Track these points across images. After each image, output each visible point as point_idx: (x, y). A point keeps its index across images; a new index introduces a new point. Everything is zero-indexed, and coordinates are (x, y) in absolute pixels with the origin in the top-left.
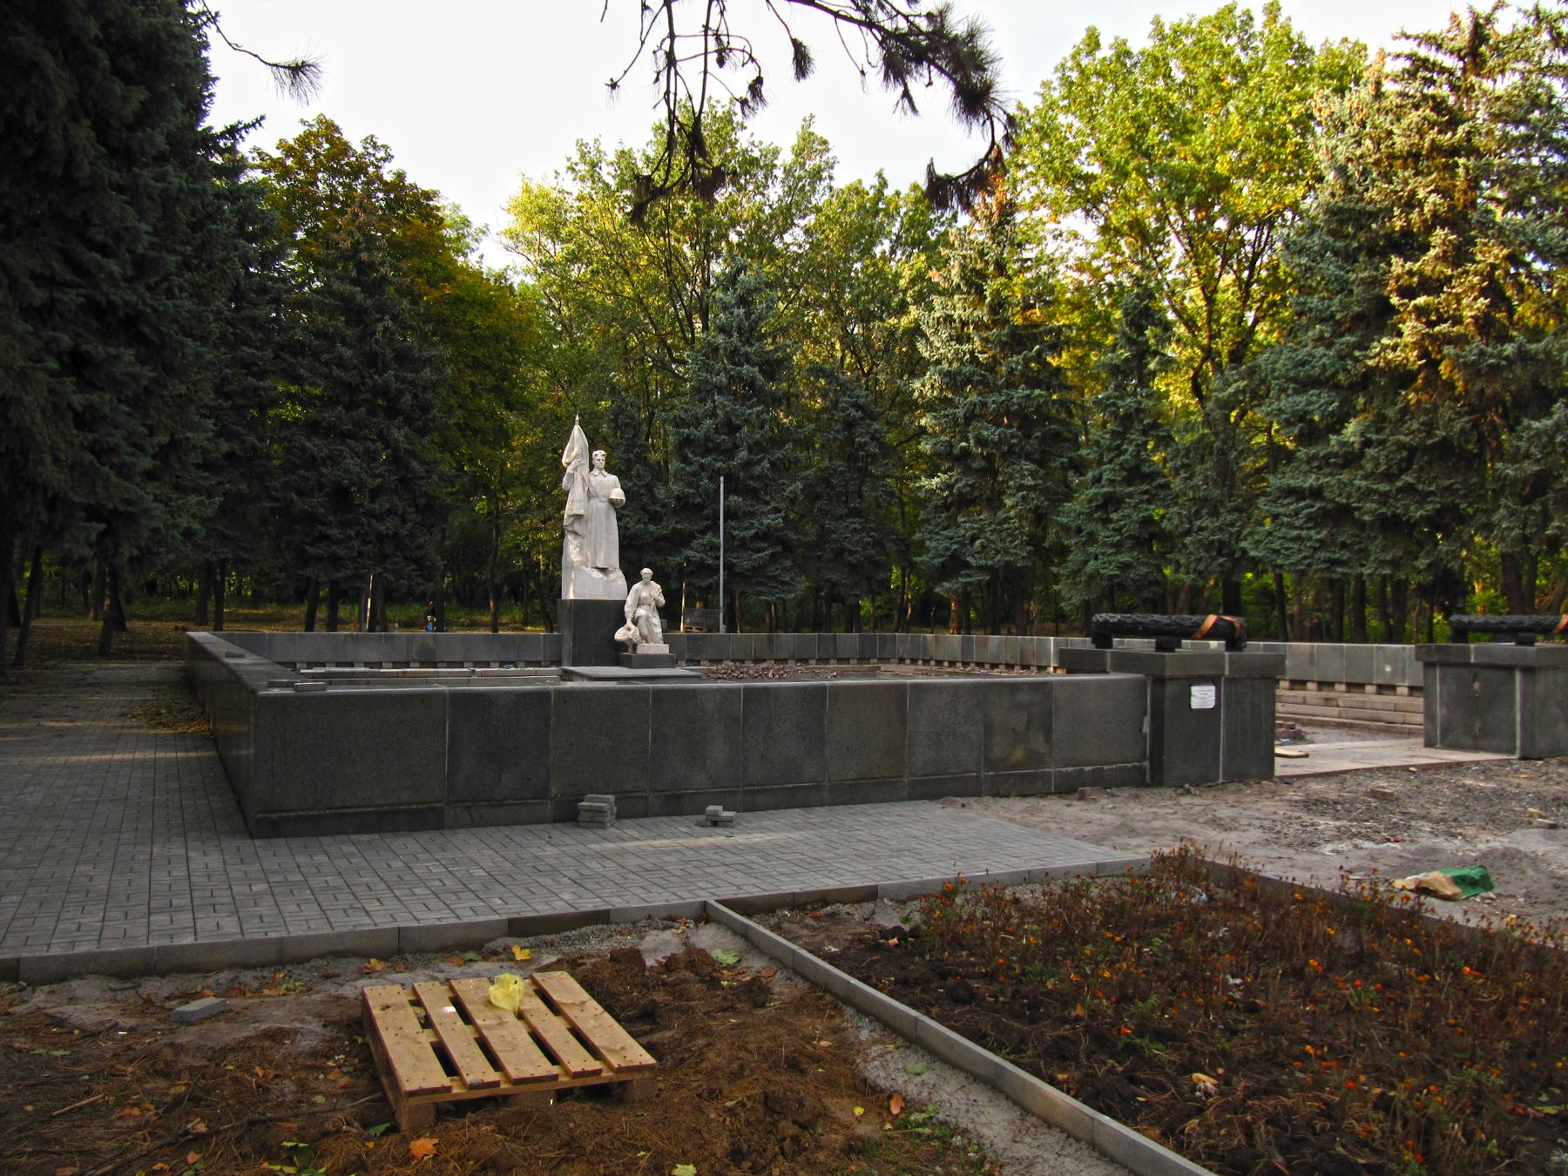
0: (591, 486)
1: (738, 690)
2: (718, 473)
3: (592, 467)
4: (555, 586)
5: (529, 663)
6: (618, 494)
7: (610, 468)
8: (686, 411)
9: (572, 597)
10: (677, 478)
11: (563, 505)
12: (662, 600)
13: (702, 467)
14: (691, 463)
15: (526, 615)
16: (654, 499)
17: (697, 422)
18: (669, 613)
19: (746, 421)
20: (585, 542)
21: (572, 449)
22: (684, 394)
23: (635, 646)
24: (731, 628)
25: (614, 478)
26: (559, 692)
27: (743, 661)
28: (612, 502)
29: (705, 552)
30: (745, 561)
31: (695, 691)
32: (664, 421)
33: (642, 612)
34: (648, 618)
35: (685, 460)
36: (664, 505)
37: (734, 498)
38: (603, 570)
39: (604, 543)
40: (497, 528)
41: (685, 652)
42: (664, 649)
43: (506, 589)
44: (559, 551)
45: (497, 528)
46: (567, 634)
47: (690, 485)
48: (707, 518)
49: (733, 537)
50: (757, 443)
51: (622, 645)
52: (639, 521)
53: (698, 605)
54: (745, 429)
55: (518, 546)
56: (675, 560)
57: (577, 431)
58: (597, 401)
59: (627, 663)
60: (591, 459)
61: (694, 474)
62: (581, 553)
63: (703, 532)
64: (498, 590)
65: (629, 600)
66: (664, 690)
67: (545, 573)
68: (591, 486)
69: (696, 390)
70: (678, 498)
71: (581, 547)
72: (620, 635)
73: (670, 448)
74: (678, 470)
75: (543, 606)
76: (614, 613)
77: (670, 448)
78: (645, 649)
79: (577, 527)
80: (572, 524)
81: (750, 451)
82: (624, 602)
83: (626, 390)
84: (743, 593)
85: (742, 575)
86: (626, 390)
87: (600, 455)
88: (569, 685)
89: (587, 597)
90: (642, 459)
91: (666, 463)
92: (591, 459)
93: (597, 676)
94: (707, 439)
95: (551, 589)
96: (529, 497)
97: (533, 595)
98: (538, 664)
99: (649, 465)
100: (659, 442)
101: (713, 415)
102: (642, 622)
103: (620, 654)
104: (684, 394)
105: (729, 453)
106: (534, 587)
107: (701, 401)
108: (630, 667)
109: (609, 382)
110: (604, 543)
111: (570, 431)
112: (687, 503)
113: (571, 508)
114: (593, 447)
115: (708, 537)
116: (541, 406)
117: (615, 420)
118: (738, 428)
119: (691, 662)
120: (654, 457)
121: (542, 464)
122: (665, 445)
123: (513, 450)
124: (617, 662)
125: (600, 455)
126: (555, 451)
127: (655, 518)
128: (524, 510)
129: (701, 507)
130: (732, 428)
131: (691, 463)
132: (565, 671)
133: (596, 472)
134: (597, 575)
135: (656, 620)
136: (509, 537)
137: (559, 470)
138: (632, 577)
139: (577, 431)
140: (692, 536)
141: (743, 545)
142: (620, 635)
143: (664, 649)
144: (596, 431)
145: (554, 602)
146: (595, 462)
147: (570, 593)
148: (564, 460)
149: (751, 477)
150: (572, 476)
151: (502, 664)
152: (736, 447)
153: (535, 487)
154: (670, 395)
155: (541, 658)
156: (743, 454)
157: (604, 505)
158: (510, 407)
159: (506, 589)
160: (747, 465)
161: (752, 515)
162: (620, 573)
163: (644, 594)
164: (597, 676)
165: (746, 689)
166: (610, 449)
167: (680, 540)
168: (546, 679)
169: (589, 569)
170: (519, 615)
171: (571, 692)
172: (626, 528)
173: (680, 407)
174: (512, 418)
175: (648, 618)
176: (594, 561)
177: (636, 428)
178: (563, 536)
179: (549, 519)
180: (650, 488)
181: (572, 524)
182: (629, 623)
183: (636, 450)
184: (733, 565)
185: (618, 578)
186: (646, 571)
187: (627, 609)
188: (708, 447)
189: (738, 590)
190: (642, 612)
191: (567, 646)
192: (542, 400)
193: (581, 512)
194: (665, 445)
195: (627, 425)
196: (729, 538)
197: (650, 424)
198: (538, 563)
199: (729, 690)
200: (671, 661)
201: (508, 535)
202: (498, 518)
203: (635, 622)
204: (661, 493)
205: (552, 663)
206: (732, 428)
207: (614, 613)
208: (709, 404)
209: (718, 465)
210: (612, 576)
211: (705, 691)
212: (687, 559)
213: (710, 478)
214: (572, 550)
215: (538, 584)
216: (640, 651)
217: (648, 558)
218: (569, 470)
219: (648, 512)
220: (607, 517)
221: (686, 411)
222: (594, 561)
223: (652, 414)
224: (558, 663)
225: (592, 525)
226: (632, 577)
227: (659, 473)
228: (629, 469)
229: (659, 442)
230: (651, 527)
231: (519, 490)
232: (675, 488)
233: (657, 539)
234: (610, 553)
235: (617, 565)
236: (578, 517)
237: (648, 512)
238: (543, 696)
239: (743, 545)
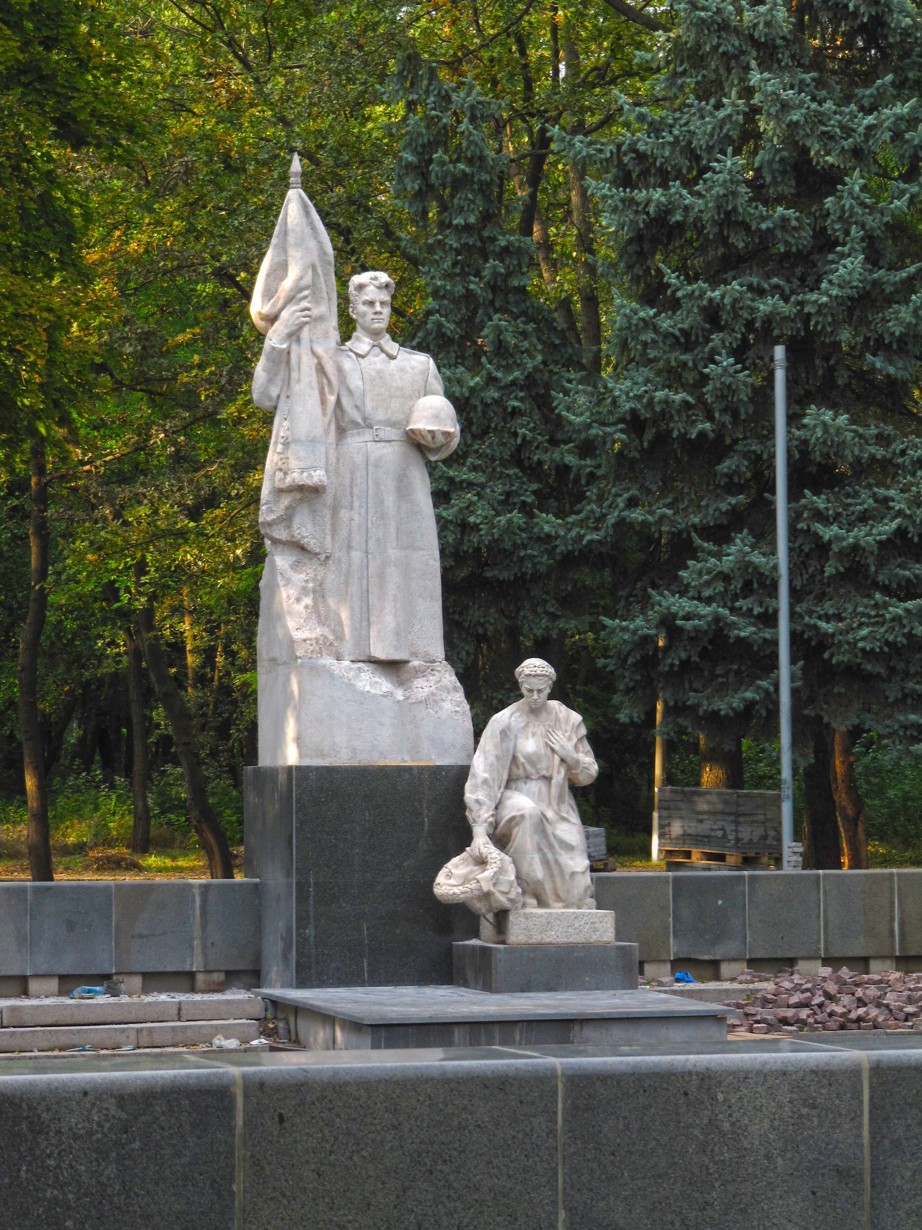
0: (347, 394)
1: (854, 1072)
2: (766, 332)
3: (347, 327)
4: (232, 721)
5: (154, 980)
6: (435, 413)
7: (407, 330)
8: (655, 129)
9: (292, 756)
10: (631, 354)
11: (253, 456)
12: (589, 764)
13: (713, 315)
14: (674, 304)
15: (143, 817)
16: (555, 429)
17: (694, 165)
18: (613, 806)
19: (857, 153)
20: (332, 578)
21: (281, 269)
22: (648, 70)
23: (501, 917)
24: (822, 853)
25: (422, 362)
26: (258, 1088)
27: (862, 963)
28: (418, 444)
29: (728, 599)
30: (861, 626)
31: (707, 1079)
32: (582, 168)
33: (522, 802)
34: (541, 825)
35: (654, 293)
36: (587, 448)
37: (821, 418)
38: (392, 667)
39: (394, 575)
40: (42, 529)
41: (680, 935)
42: (597, 926)
43: (74, 734)
44: (247, 606)
45: (42, 529)
46: (276, 879)
47: (673, 377)
48: (732, 486)
49: (822, 548)
50: (897, 228)
51: (459, 916)
52: (507, 502)
53: (710, 776)
54: (856, 181)
55: (111, 592)
56: (630, 627)
57: (295, 207)
58: (357, 108)
59: (479, 972)
60: (344, 302)
61: (686, 341)
62: (319, 613)
63: (720, 534)
64: (49, 735)
65: (480, 765)
66: (905, 874)
67: (202, 680)
68: (347, 394)
69: (689, 56)
70: (634, 423)
71: (319, 592)
72: (452, 880)
73: (606, 252)
74: (631, 329)
75: (199, 789)
76: (433, 809)
77: (606, 252)
78: (531, 926)
79: (304, 528)
80: (287, 519)
81: (873, 258)
82: (462, 773)
83: (454, 65)
84: (856, 733)
85: (852, 672)
86: (454, 65)
87: (372, 285)
88: (290, 1062)
89: (343, 758)
90: (507, 295)
91: (591, 301)
92: (344, 302)
93: (355, 1034)
94: (729, 219)
95: (223, 731)
96: (144, 431)
97: (164, 751)
98: (186, 980)
99: (537, 316)
100: (564, 236)
101: (747, 136)
102: (524, 837)
103: (448, 942)
104: (648, 70)
105: (804, 264)
106: (155, 724)
107: (703, 94)
108: (488, 987)
109: (394, 39)
110: (394, 575)
111: (271, 210)
112: (663, 438)
113: (291, 458)
114: (349, 257)
115: (739, 547)
116: (177, 126)
117: (421, 170)
118: (831, 180)
119: (685, 965)
120: (551, 284)
121: (182, 321)
122: (586, 244)
123: (86, 277)
124: (445, 971)
125: (372, 285)
126: (224, 276)
127: (561, 490)
128: (130, 471)
129: (711, 449)
130: (810, 181)
131: (674, 304)
132: (275, 1004)
133: (361, 343)
134: (372, 683)
135: (570, 829)
136: (81, 563)
137: (237, 341)
138: (488, 689)
139: (295, 207)
140: (683, 549)
141: (856, 573)
142: (452, 880)
143: (597, 926)
144: (360, 204)
145: (234, 773)
146: (359, 309)
147: (287, 745)
148: (257, 307)
149: (880, 345)
150: (283, 359)
151: (67, 983)
152: (826, 243)
153: (161, 393)
154: (602, 76)
155: (195, 964)
156: (849, 267)
157: (390, 453)
158: (71, 133)
159: (74, 734)
160: (864, 302)
161: (885, 469)
162: (449, 677)
163: (529, 745)
164: (355, 1034)
165: (877, 1069)
166: (407, 265)
167: (651, 561)
168: (210, 1040)
169: (349, 664)
170: (119, 822)
171: (299, 1088)
172: (464, 527)
173: (635, 115)
174: (84, 168)
175: (541, 825)
176: (362, 638)
177: (492, 191)
178: (257, 556)
179: (211, 502)
180: (539, 392)
181: (287, 519)
182: (481, 842)
183: (492, 265)
184: (824, 642)
185: (441, 692)
186: (535, 669)
187: (472, 794)
188: (731, 248)
189: (841, 726)
190: (522, 802)
191: (280, 922)
192: (179, 107)
193: (318, 476)
194: (586, 244)
195: (459, 183)
196: (809, 550)
197: (535, 178)
198: (178, 648)
199: (824, 1076)
200: (630, 969)
201: (79, 557)
202: (43, 498)
203: (501, 839)
204: (576, 405)
205: (231, 978)
206: (810, 181)
207: (433, 809)
208: (732, 102)
209: (765, 306)
210: (422, 687)
211: (742, 1076)
212: (667, 622)
213: (739, 353)
214: (292, 605)
215: (179, 715)
216: (517, 933)
217: (541, 627)
218: (274, 339)
219: (534, 471)
220: (403, 491)
221: (655, 129)
222: (362, 638)
223: (543, 141)
224: (253, 976)
225: (352, 517)
226: (488, 689)
227: (567, 339)
228: (471, 327)
229: (564, 236)
230: (547, 523)
231: (110, 408)
232: (627, 388)
233: (570, 560)
234: (414, 616)
235: (438, 650)
236: (309, 493)
237: (534, 471)
238: (210, 1100)
239: (856, 573)
